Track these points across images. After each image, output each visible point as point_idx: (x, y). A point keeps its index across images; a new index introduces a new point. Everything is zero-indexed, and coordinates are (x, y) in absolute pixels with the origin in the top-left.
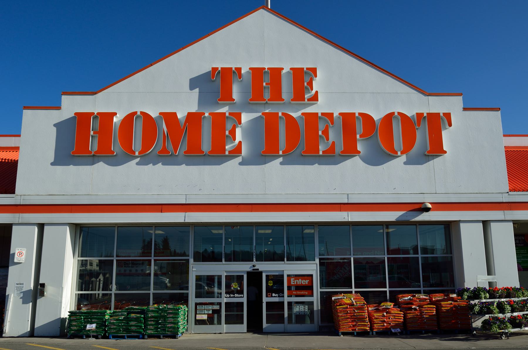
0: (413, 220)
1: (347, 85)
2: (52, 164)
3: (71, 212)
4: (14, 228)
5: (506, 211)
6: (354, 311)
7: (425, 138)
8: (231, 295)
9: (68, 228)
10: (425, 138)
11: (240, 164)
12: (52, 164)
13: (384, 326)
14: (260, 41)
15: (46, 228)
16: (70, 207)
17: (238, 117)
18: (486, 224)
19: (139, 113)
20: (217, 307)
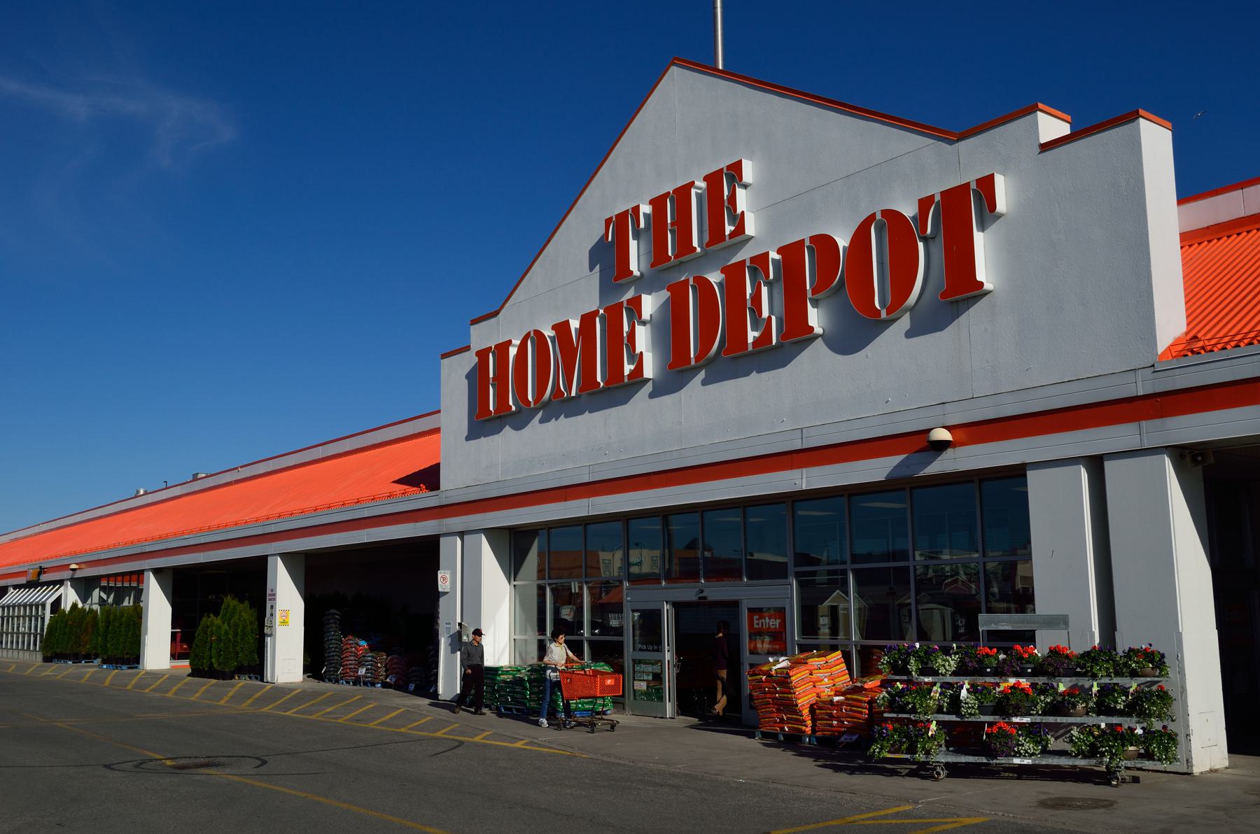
0: (921, 474)
1: (800, 171)
2: (468, 439)
3: (791, 466)
4: (442, 540)
5: (1144, 423)
6: (24, 634)
7: (912, 267)
8: (650, 647)
9: (1167, 461)
10: (912, 267)
11: (652, 396)
12: (468, 439)
13: (832, 725)
14: (685, 128)
15: (1108, 465)
16: (832, 450)
17: (636, 304)
18: (1096, 465)
19: (879, 216)
20: (657, 669)
